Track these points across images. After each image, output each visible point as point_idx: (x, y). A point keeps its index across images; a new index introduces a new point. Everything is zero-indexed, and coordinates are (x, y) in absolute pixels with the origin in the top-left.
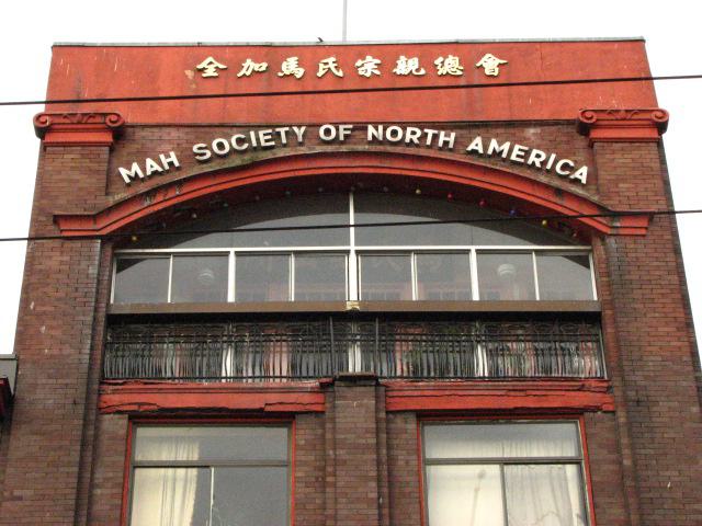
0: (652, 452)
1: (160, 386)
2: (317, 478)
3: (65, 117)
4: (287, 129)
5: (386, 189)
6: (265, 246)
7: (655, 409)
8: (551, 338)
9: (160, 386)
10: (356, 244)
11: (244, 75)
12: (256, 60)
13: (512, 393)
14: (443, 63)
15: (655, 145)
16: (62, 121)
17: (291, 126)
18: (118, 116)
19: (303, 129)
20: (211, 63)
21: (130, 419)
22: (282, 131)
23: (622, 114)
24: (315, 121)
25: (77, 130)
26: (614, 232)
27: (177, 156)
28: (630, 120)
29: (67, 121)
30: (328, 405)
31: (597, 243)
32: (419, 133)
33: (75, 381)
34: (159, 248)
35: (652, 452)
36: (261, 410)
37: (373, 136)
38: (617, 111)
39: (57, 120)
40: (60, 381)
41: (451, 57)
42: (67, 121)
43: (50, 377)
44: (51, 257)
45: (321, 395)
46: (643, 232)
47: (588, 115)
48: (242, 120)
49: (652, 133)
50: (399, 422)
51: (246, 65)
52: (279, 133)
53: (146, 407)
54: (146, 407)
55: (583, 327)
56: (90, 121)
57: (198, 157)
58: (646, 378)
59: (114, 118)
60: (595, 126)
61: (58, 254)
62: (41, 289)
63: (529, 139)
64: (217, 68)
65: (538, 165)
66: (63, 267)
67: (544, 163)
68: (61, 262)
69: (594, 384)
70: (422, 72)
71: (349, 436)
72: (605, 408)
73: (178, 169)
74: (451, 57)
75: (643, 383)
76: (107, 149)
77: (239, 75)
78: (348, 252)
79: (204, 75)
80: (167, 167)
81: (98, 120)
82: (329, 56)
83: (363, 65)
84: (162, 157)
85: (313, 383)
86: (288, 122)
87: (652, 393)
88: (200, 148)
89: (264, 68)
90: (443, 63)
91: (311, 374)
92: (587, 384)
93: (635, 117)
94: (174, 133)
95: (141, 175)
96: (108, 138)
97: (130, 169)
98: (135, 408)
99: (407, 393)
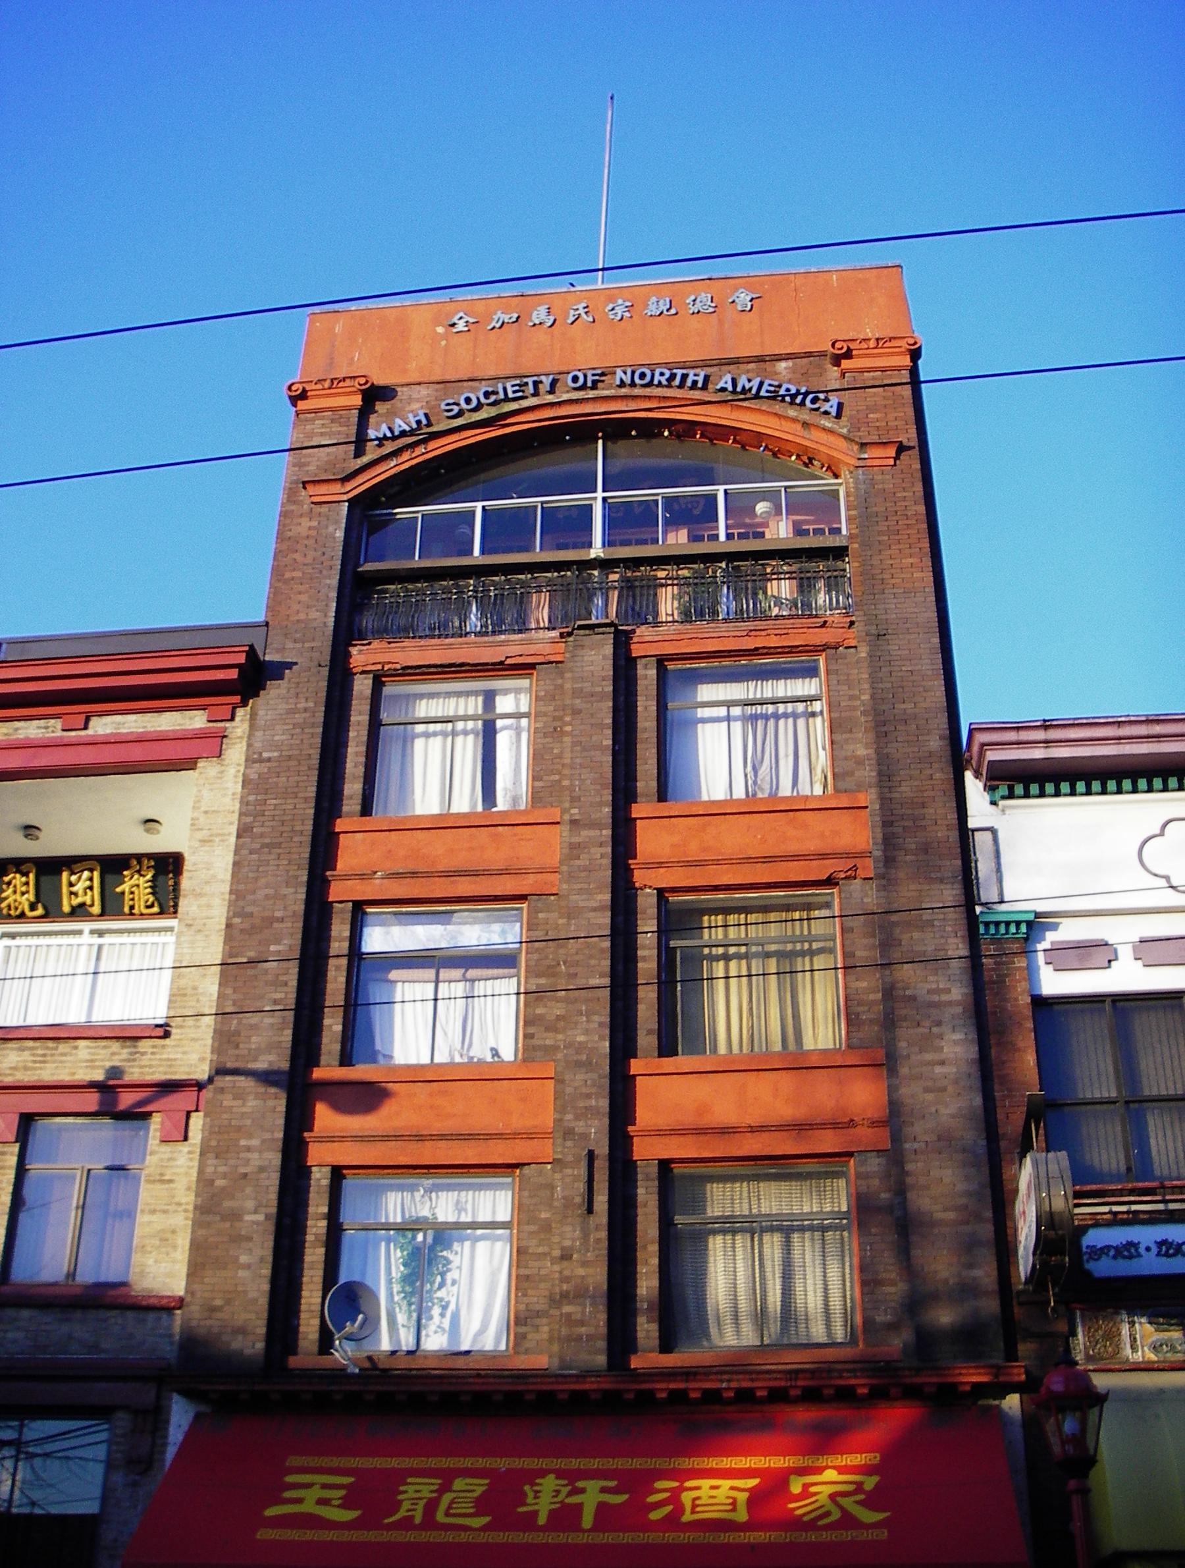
2: (555, 729)
11: (494, 328)
20: (461, 318)
37: (622, 380)
63: (780, 373)
68: (310, 528)
74: (703, 295)
84: (411, 416)
90: (694, 301)
98: (379, 667)
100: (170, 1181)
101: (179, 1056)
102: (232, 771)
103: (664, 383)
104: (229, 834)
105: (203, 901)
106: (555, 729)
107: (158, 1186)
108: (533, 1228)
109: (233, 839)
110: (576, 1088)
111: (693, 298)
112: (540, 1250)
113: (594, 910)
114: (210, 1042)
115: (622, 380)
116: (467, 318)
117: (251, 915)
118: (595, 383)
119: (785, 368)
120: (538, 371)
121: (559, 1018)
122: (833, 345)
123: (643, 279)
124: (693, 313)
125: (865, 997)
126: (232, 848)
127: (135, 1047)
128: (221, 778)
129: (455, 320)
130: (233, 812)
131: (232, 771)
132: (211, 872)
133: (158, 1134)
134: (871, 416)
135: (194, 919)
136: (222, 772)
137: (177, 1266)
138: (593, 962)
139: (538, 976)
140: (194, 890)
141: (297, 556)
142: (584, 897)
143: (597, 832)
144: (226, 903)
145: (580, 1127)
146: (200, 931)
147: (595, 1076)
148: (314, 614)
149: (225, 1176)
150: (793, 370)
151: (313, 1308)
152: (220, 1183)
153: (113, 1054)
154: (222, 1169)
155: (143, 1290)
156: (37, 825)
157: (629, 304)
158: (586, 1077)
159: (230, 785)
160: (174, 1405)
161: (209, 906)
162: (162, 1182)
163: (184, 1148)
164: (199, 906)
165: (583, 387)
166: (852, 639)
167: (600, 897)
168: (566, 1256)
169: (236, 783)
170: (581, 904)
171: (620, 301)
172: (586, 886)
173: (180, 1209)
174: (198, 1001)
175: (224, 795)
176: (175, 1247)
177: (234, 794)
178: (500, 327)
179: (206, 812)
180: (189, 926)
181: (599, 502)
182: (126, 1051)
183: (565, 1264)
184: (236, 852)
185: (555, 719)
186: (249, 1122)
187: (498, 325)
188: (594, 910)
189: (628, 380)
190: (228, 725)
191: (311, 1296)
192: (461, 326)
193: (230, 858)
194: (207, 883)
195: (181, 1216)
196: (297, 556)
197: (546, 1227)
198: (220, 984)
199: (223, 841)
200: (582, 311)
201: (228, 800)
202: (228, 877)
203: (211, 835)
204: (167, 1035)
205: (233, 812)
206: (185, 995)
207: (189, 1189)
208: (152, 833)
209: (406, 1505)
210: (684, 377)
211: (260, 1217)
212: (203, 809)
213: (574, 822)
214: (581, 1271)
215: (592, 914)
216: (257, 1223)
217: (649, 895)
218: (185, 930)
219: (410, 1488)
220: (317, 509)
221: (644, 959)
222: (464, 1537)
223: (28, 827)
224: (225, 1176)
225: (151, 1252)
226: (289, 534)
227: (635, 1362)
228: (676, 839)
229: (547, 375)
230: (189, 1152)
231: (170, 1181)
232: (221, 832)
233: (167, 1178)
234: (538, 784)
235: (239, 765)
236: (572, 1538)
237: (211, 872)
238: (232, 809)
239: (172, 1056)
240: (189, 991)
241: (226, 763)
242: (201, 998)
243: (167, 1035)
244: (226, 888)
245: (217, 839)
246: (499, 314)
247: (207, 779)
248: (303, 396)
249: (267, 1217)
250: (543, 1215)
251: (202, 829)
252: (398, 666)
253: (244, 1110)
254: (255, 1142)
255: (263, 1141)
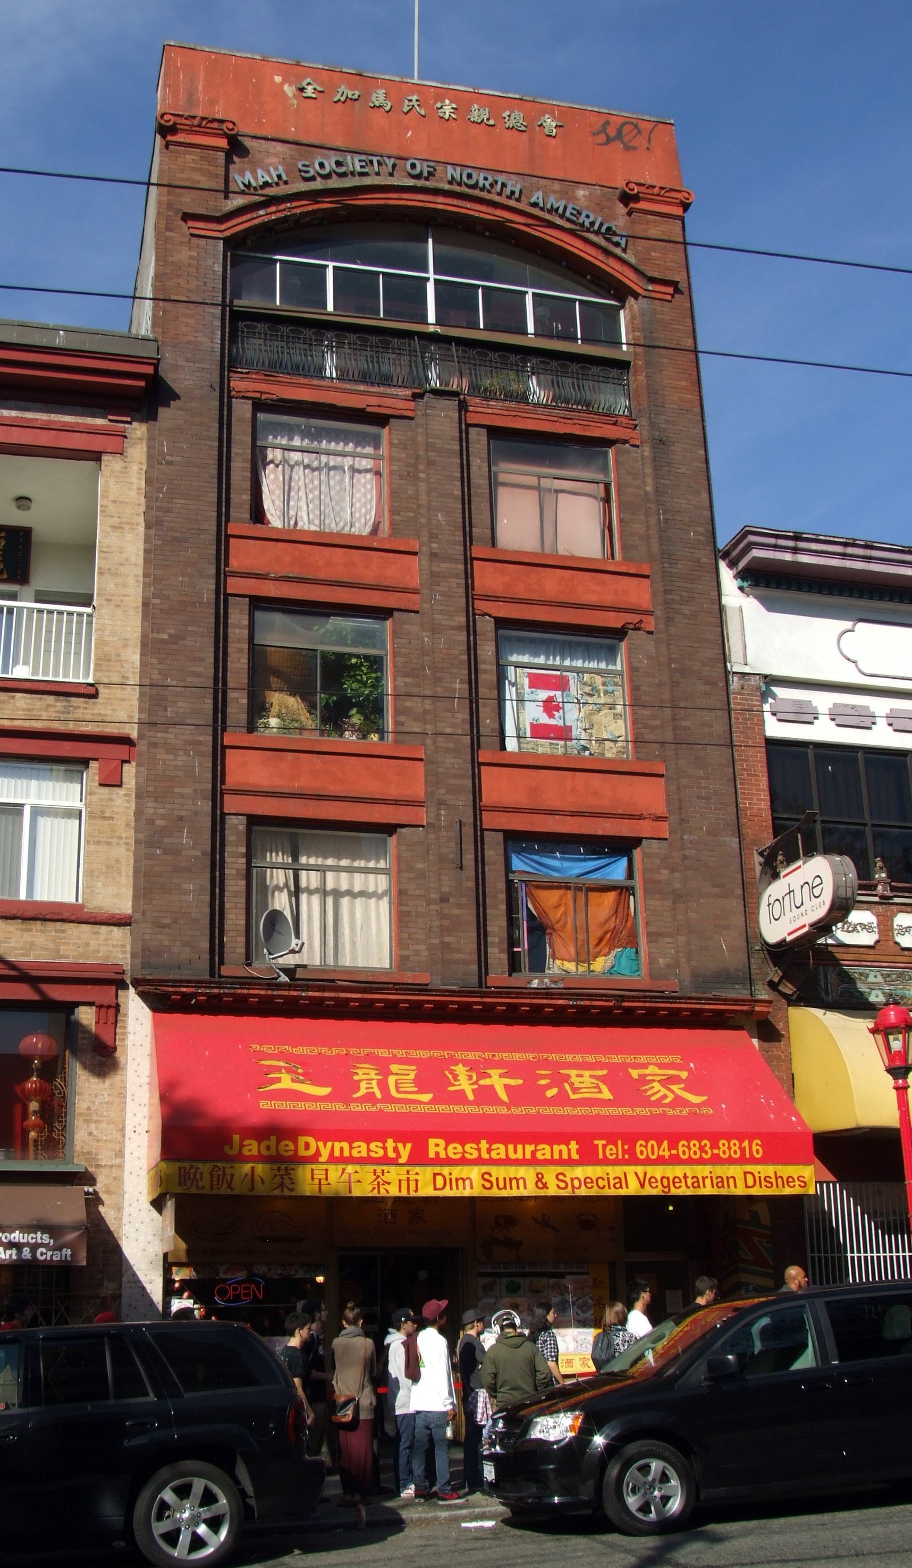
0: (669, 482)
1: (278, 379)
2: (409, 473)
3: (186, 118)
4: (379, 158)
5: (487, 234)
6: (357, 264)
7: (672, 448)
8: (570, 375)
9: (278, 379)
10: (435, 273)
11: (339, 100)
12: (352, 88)
13: (562, 420)
14: (509, 116)
15: (679, 222)
16: (184, 122)
17: (382, 156)
18: (234, 124)
19: (392, 160)
20: (309, 84)
21: (253, 404)
22: (375, 159)
23: (656, 191)
24: (402, 154)
25: (197, 133)
26: (647, 294)
27: (284, 170)
28: (662, 196)
29: (188, 122)
30: (418, 413)
31: (631, 301)
32: (490, 180)
33: (208, 366)
34: (262, 253)
35: (669, 482)
36: (363, 410)
37: (452, 177)
38: (654, 187)
39: (179, 120)
40: (197, 365)
41: (516, 112)
42: (188, 122)
43: (188, 360)
44: (180, 252)
45: (413, 403)
46: (669, 298)
47: (167, 117)
48: (339, 143)
49: (678, 211)
50: (473, 431)
51: (341, 90)
52: (371, 162)
53: (267, 396)
54: (267, 396)
55: (615, 372)
56: (209, 125)
57: (303, 174)
58: (667, 422)
59: (231, 126)
60: (636, 198)
61: (187, 249)
62: (174, 280)
63: (579, 200)
64: (315, 89)
65: (587, 224)
66: (192, 261)
67: (592, 224)
68: (190, 257)
69: (625, 421)
70: (492, 122)
71: (437, 441)
72: (632, 442)
73: (286, 183)
74: (516, 112)
75: (664, 426)
76: (223, 154)
77: (335, 100)
78: (428, 279)
79: (304, 95)
80: (276, 179)
81: (215, 125)
82: (413, 95)
83: (442, 107)
84: (272, 169)
85: (408, 392)
86: (379, 151)
87: (671, 435)
88: (304, 166)
89: (356, 97)
90: (509, 116)
91: (400, 384)
92: (620, 420)
93: (209, 125)
94: (280, 147)
95: (254, 184)
96: (223, 143)
97: (243, 176)
98: (258, 395)
99: (480, 410)
100: (111, 818)
101: (109, 712)
102: (135, 468)
103: (488, 186)
104: (138, 524)
105: (119, 580)
106: (409, 473)
107: (100, 822)
108: (412, 875)
109: (141, 529)
110: (446, 769)
111: (508, 113)
112: (418, 892)
113: (453, 628)
114: (136, 703)
115: (452, 177)
116: (315, 86)
117: (168, 597)
118: (430, 174)
119: (584, 196)
120: (384, 152)
121: (426, 712)
122: (627, 184)
123: (581, 104)
124: (508, 128)
125: (649, 722)
126: (142, 536)
127: (69, 701)
128: (126, 473)
129: (304, 84)
130: (139, 505)
131: (135, 468)
132: (124, 555)
133: (97, 778)
134: (653, 254)
135: (112, 595)
136: (126, 467)
137: (123, 890)
138: (454, 671)
139: (407, 675)
140: (109, 569)
141: (181, 281)
142: (445, 617)
143: (453, 566)
144: (141, 585)
145: (451, 799)
146: (118, 606)
147: (460, 761)
148: (202, 338)
149: (163, 817)
150: (589, 198)
151: (238, 928)
152: (161, 822)
153: (49, 706)
154: (162, 811)
155: (95, 908)
156: (29, 496)
157: (319, 89)
158: (454, 761)
159: (134, 480)
160: (130, 1002)
161: (125, 585)
162: (104, 818)
163: (121, 792)
164: (117, 585)
165: (418, 177)
166: (635, 436)
167: (457, 619)
168: (444, 899)
169: (140, 479)
170: (444, 622)
171: (447, 102)
172: (446, 608)
173: (122, 842)
174: (122, 666)
175: (130, 489)
176: (120, 873)
177: (139, 489)
178: (344, 102)
179: (115, 502)
180: (109, 600)
181: (432, 281)
182: (59, 704)
183: (444, 905)
184: (146, 541)
185: (408, 465)
186: (181, 774)
187: (343, 99)
188: (453, 628)
189: (458, 177)
190: (127, 426)
191: (234, 919)
192: (309, 91)
193: (141, 545)
194: (122, 564)
195: (123, 849)
196: (181, 281)
197: (422, 875)
198: (141, 655)
199: (133, 529)
200: (415, 103)
201: (133, 493)
202: (141, 561)
203: (121, 523)
204: (95, 696)
205: (139, 505)
206: (109, 660)
207: (128, 825)
208: (24, 509)
209: (363, 1085)
210: (504, 185)
211: (199, 853)
212: (112, 497)
213: (433, 555)
214: (456, 912)
215: (450, 632)
216: (196, 858)
217: (488, 621)
218: (105, 603)
219: (360, 1072)
220: (195, 240)
221: (486, 672)
222: (412, 1108)
223: (19, 498)
224: (163, 817)
225: (99, 877)
226: (171, 259)
227: (225, 971)
228: (507, 579)
229: (389, 157)
230: (126, 795)
231: (111, 818)
232: (129, 521)
233: (107, 815)
234: (396, 517)
235: (141, 463)
236: (492, 1110)
237: (124, 555)
238: (138, 502)
239: (102, 712)
240: (113, 657)
241: (128, 460)
242: (125, 665)
243: (95, 696)
244: (140, 571)
245: (127, 527)
246: (342, 88)
247: (112, 472)
248: (173, 129)
249: (203, 853)
250: (419, 866)
251: (112, 517)
252: (275, 397)
253: (176, 763)
254: (188, 791)
255: (195, 791)
